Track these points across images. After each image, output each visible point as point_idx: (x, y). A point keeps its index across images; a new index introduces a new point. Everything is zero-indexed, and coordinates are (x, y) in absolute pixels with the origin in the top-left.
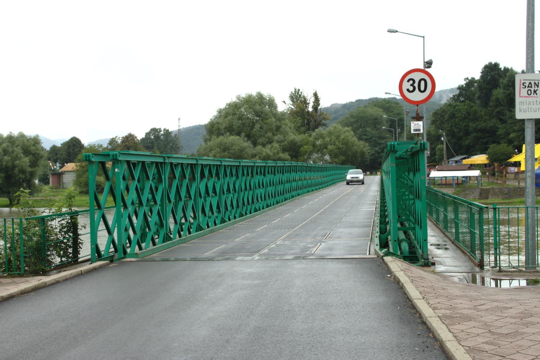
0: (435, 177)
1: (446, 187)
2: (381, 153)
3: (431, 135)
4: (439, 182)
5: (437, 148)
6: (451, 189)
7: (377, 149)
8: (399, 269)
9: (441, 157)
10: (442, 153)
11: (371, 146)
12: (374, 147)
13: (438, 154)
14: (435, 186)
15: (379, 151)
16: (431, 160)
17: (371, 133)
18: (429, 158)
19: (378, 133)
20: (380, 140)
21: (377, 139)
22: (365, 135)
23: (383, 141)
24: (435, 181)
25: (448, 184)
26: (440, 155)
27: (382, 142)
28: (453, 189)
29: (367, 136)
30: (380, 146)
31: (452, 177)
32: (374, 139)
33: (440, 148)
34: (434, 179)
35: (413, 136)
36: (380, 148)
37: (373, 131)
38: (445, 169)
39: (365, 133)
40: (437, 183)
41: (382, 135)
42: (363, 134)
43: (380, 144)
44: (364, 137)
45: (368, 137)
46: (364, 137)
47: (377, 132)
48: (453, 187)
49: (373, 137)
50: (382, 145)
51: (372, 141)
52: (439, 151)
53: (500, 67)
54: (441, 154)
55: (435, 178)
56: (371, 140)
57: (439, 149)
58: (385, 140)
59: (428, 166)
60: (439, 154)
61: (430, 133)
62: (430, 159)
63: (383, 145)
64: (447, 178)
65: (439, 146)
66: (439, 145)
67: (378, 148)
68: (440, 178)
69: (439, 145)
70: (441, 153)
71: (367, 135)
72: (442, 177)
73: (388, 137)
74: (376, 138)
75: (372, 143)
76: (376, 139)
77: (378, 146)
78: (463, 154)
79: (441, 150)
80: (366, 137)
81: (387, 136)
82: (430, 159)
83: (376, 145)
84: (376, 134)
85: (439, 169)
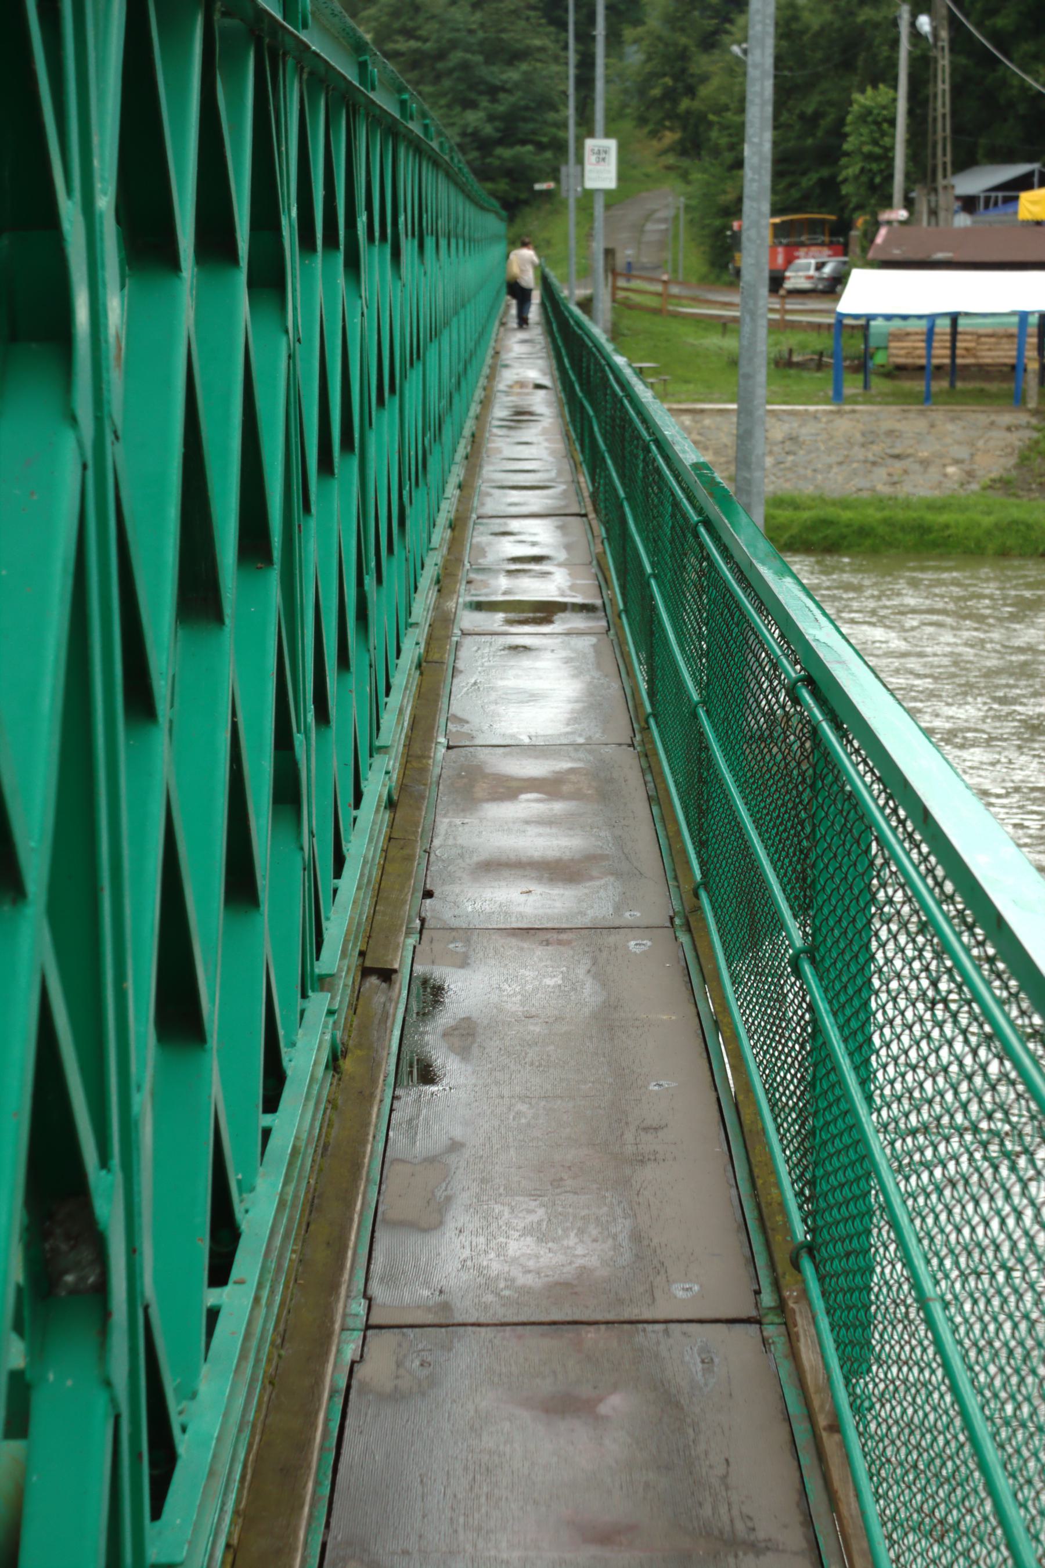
0: (870, 317)
1: (952, 396)
2: (500, 142)
3: (802, 33)
4: (899, 353)
5: (855, 108)
6: (1007, 418)
7: (473, 118)
8: (439, 747)
9: (874, 166)
10: (887, 141)
11: (443, 102)
12: (457, 109)
13: (859, 151)
14: (866, 386)
15: (488, 130)
16: (795, 193)
17: (443, 23)
18: (787, 180)
19: (482, 25)
20: (495, 69)
21: (479, 58)
22: (409, 34)
23: (513, 75)
24: (873, 343)
25: (983, 372)
26: (870, 157)
27: (504, 77)
28: (1023, 418)
29: (418, 38)
30: (494, 100)
31: (1013, 314)
32: (457, 56)
33: (869, 112)
34: (866, 327)
35: (686, 48)
36: (491, 118)
37: (453, 9)
38: (940, 256)
39: (410, 24)
40: (880, 359)
41: (504, 36)
42: (396, 25)
43: (494, 91)
44: (403, 45)
45: (428, 45)
46: (403, 45)
47: (478, 16)
48: (1018, 399)
49: (454, 45)
50: (502, 96)
51: (450, 72)
52: (864, 130)
53: (594, 33)
54: (877, 150)
55: (873, 323)
56: (440, 66)
57: (866, 115)
58: (524, 67)
59: (779, 231)
60: (866, 149)
61: (795, 18)
62: (791, 185)
63: (512, 99)
64: (962, 322)
65: (864, 99)
66: (863, 91)
67: (481, 114)
68: (923, 325)
69: (863, 91)
70: (875, 142)
71: (422, 33)
72: (932, 318)
73: (542, 49)
74: (473, 53)
75: (447, 83)
76: (469, 56)
77: (484, 102)
78: (1009, 157)
79: (877, 124)
80: (413, 44)
81: (537, 42)
82: (791, 185)
83: (473, 95)
84: (471, 32)
85: (897, 253)
